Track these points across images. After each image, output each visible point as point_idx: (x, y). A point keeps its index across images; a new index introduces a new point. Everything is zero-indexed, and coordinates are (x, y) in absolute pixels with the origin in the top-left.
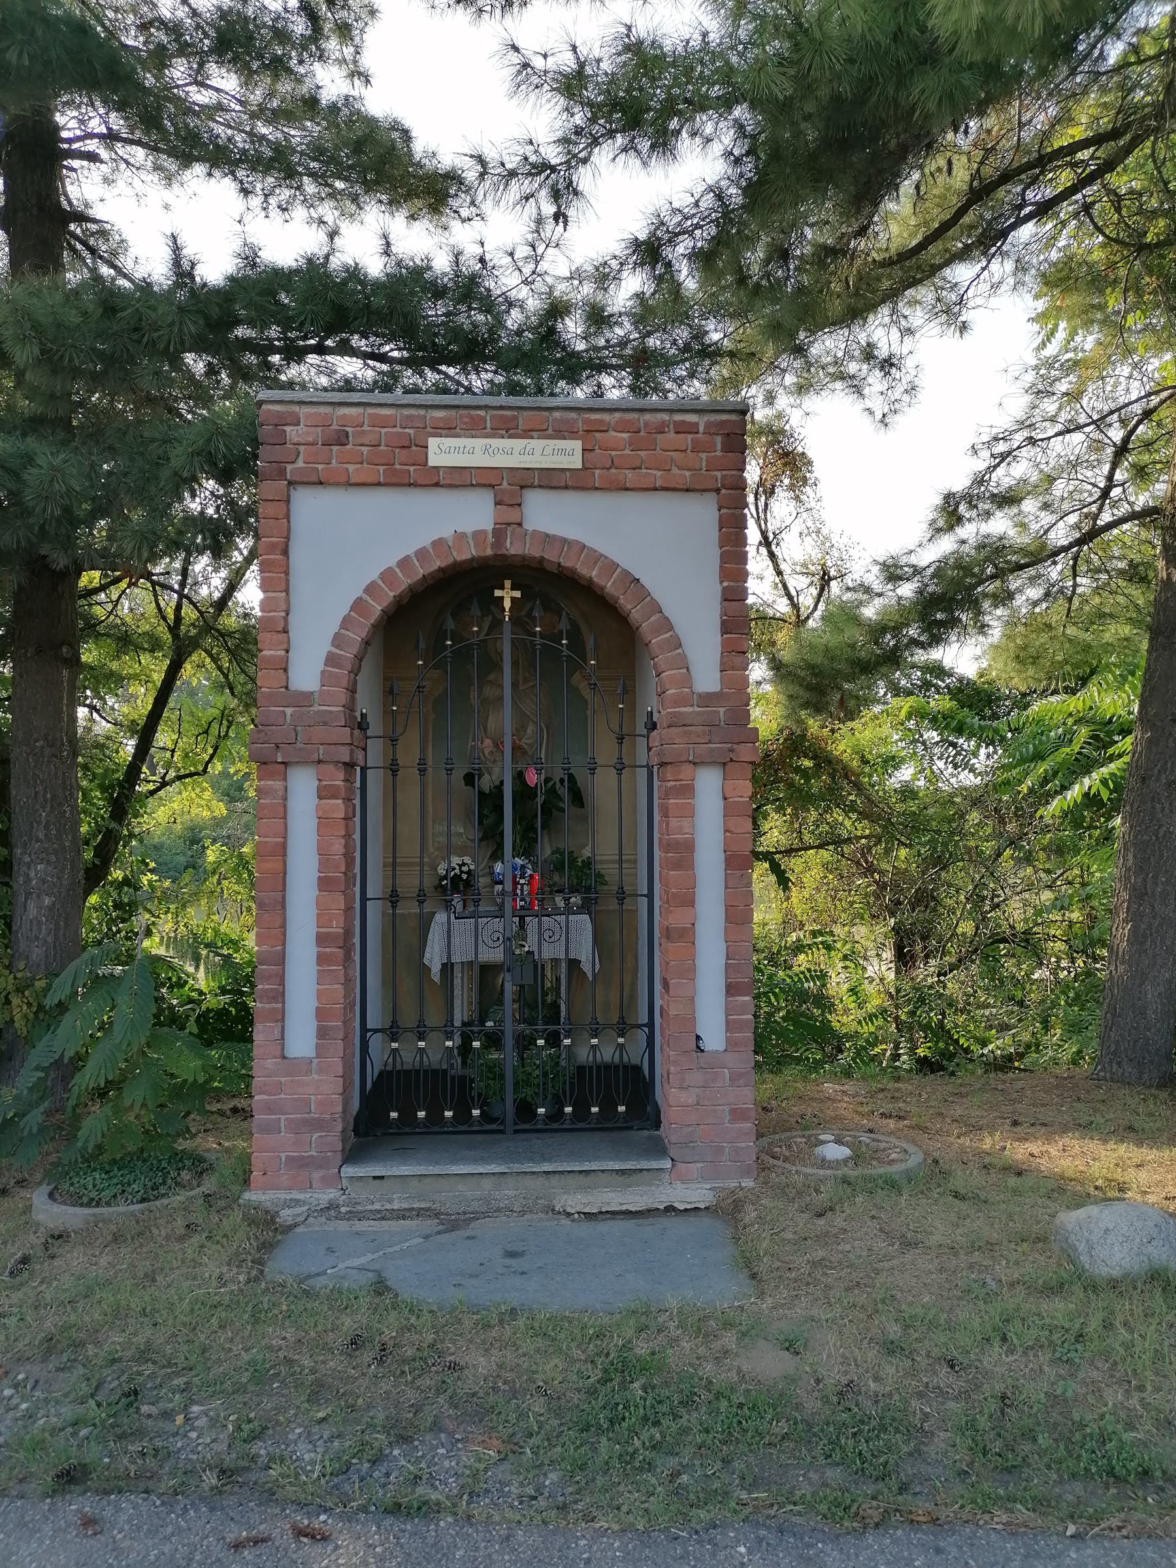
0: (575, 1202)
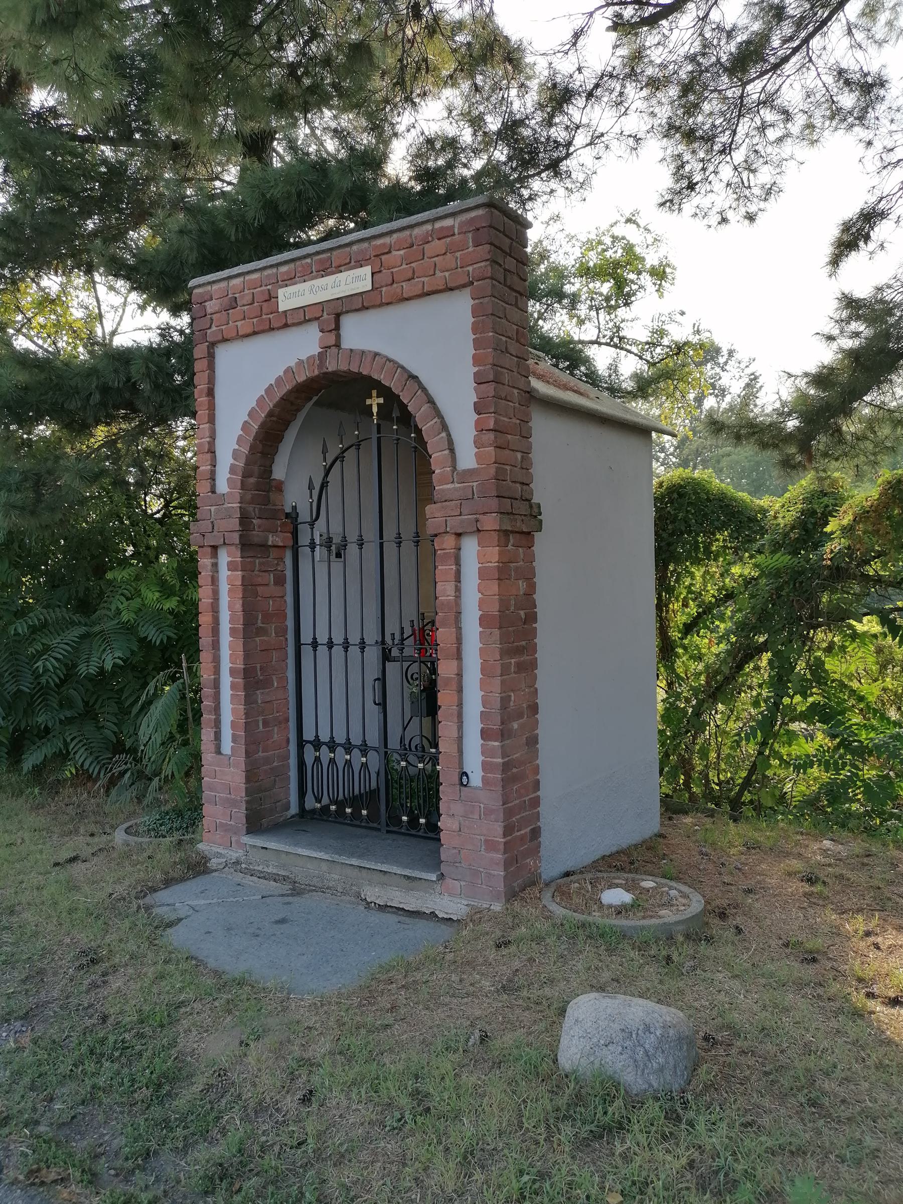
0: (373, 893)
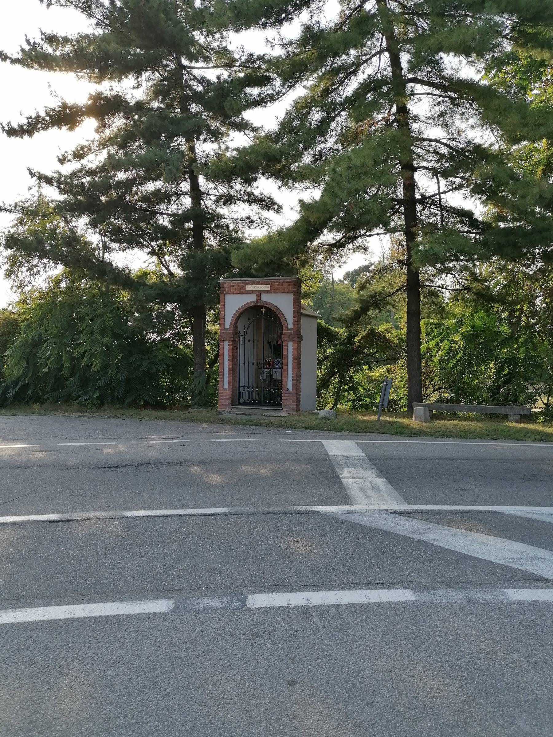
0: (266, 414)
